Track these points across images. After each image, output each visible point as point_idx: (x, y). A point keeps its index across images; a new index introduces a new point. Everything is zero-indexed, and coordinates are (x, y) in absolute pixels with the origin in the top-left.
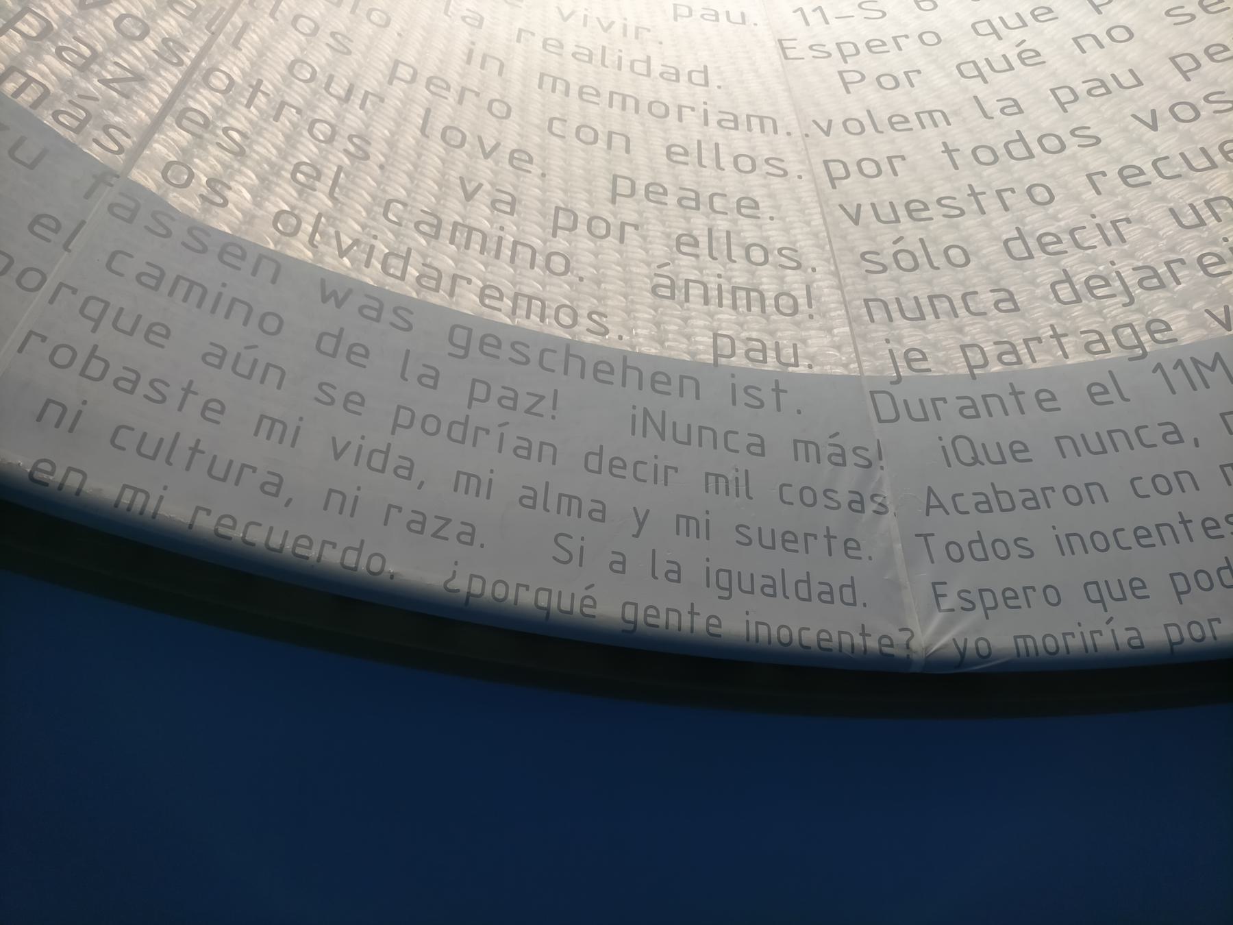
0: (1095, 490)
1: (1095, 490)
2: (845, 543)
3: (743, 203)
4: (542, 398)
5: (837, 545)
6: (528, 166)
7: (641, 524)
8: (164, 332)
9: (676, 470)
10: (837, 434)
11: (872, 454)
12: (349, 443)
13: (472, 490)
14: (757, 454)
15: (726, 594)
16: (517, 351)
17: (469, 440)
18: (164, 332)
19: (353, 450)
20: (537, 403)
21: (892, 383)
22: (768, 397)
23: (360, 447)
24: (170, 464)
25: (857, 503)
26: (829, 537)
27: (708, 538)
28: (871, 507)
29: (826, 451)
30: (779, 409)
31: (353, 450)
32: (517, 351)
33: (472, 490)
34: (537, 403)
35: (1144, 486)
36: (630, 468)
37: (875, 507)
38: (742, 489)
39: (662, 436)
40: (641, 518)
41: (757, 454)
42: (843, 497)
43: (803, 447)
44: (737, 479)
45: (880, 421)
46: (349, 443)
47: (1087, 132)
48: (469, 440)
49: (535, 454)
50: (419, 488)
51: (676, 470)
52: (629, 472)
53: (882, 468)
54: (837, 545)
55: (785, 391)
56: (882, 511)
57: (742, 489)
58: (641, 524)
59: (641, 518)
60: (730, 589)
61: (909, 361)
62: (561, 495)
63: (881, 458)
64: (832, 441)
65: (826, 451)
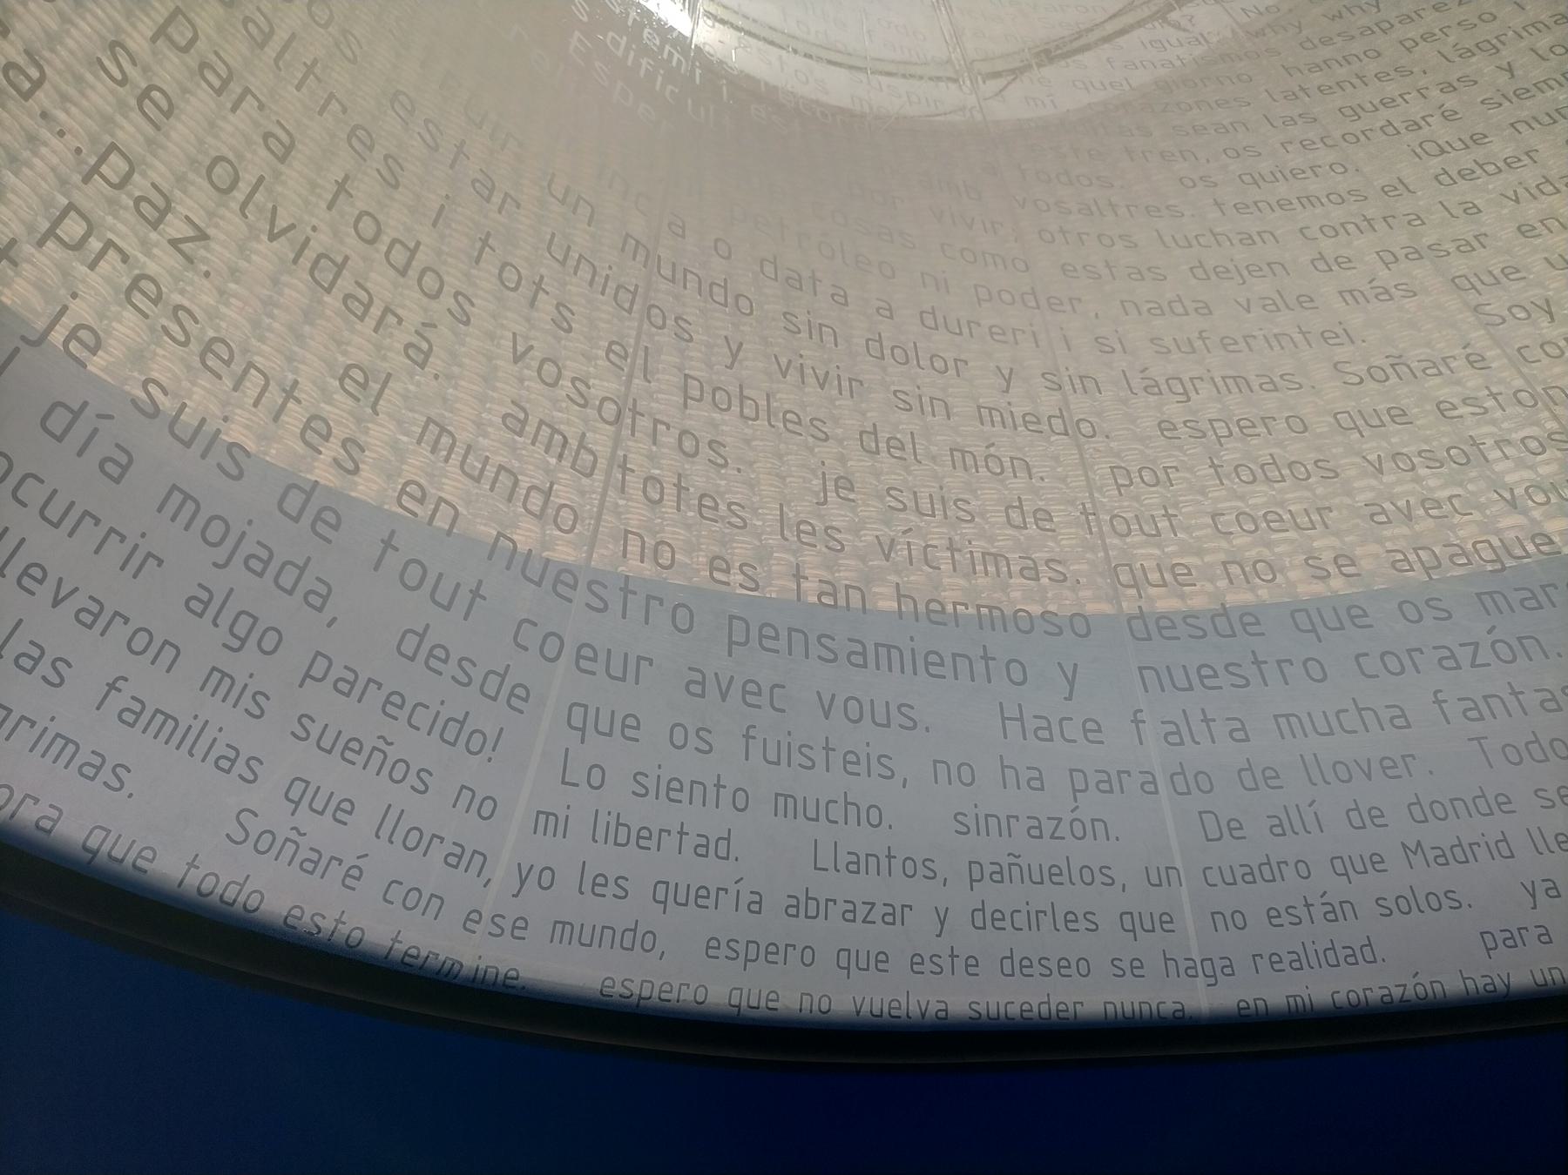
0: (1099, 826)
1: (1099, 826)
3: (360, 133)
6: (480, 177)
8: (92, 343)
9: (160, 562)
13: (1298, 731)
14: (254, 572)
15: (236, 644)
16: (232, 457)
17: (631, 676)
18: (92, 343)
24: (216, 625)
32: (232, 457)
35: (1214, 877)
40: (62, 594)
41: (254, 572)
47: (467, 306)
48: (631, 676)
49: (1116, 787)
50: (329, 625)
51: (160, 562)
55: (635, 593)
58: (942, 924)
59: (62, 594)
60: (243, 641)
61: (72, 335)
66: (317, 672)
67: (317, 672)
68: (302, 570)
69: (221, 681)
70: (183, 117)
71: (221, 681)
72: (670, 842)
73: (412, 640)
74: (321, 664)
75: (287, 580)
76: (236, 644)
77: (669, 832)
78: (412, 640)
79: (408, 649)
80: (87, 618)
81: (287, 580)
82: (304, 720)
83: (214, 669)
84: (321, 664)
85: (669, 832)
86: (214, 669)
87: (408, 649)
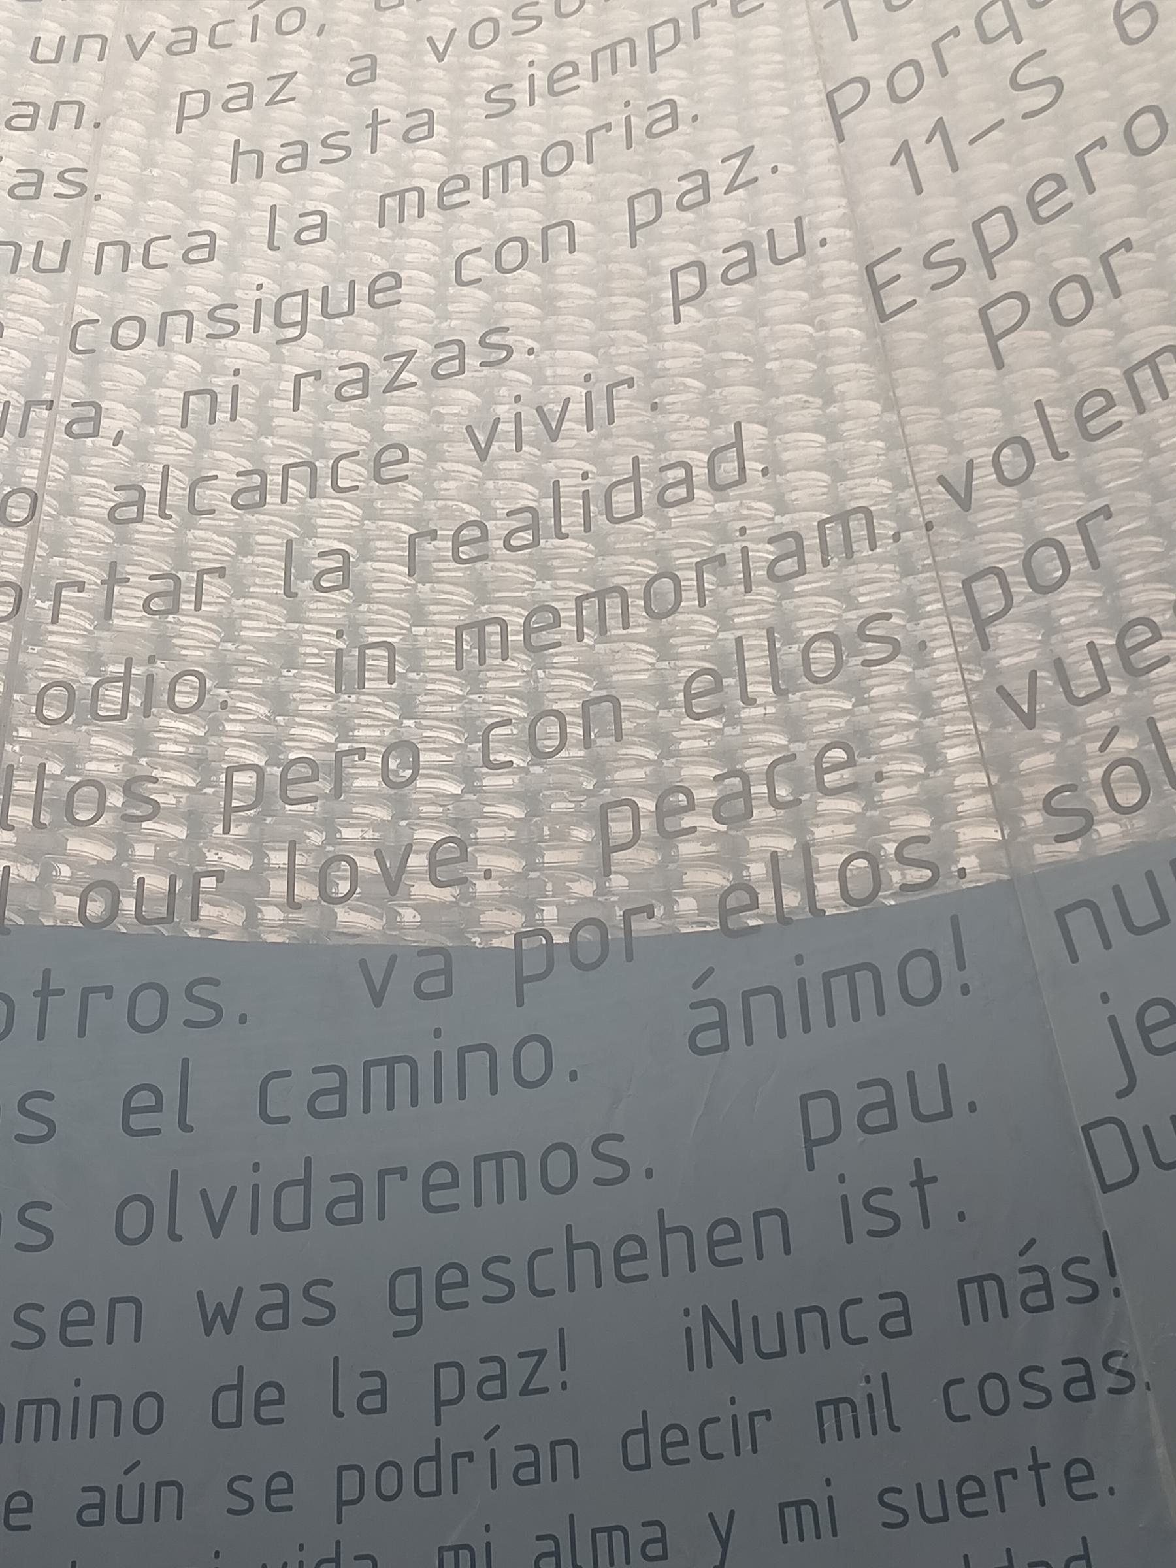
2: (1067, 1471)
4: (542, 1354)
5: (1052, 1478)
7: (724, 1543)
9: (767, 1414)
10: (1032, 1242)
11: (1095, 1270)
12: (233, 1190)
13: (402, 1095)
15: (410, 1322)
19: (243, 1201)
20: (538, 1363)
21: (1120, 1095)
22: (905, 1202)
23: (256, 1188)
25: (1080, 1385)
26: (1036, 1467)
27: (835, 1534)
28: (1104, 1381)
29: (1016, 1284)
30: (926, 1224)
31: (243, 1201)
33: (402, 1095)
34: (538, 1363)
36: (694, 1439)
37: (1111, 1380)
38: (881, 1412)
39: (738, 1355)
42: (1054, 1378)
43: (978, 1290)
44: (870, 1396)
45: (1106, 1188)
46: (233, 1190)
51: (767, 1414)
52: (692, 1449)
53: (1117, 1292)
54: (1052, 1478)
56: (1126, 1385)
57: (881, 1412)
58: (724, 1543)
60: (417, 1311)
62: (595, 1532)
63: (1113, 1273)
64: (1024, 1262)
65: (1016, 1284)
66: (449, 1390)
67: (449, 1390)
68: (306, 1182)
69: (837, 1410)
70: (248, 262)
71: (837, 1410)
72: (1021, 1490)
73: (228, 1400)
74: (449, 1377)
75: (292, 1212)
76: (410, 1322)
77: (1013, 1473)
78: (228, 1400)
79: (227, 1413)
80: (330, 1103)
81: (292, 1212)
82: (888, 1498)
83: (962, 1283)
84: (449, 1377)
85: (1013, 1473)
86: (962, 1283)
87: (227, 1413)
